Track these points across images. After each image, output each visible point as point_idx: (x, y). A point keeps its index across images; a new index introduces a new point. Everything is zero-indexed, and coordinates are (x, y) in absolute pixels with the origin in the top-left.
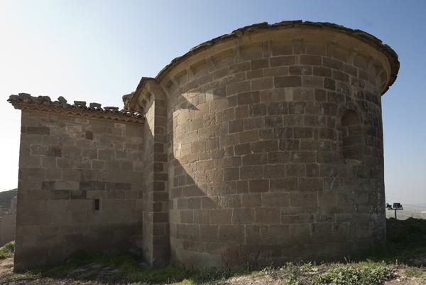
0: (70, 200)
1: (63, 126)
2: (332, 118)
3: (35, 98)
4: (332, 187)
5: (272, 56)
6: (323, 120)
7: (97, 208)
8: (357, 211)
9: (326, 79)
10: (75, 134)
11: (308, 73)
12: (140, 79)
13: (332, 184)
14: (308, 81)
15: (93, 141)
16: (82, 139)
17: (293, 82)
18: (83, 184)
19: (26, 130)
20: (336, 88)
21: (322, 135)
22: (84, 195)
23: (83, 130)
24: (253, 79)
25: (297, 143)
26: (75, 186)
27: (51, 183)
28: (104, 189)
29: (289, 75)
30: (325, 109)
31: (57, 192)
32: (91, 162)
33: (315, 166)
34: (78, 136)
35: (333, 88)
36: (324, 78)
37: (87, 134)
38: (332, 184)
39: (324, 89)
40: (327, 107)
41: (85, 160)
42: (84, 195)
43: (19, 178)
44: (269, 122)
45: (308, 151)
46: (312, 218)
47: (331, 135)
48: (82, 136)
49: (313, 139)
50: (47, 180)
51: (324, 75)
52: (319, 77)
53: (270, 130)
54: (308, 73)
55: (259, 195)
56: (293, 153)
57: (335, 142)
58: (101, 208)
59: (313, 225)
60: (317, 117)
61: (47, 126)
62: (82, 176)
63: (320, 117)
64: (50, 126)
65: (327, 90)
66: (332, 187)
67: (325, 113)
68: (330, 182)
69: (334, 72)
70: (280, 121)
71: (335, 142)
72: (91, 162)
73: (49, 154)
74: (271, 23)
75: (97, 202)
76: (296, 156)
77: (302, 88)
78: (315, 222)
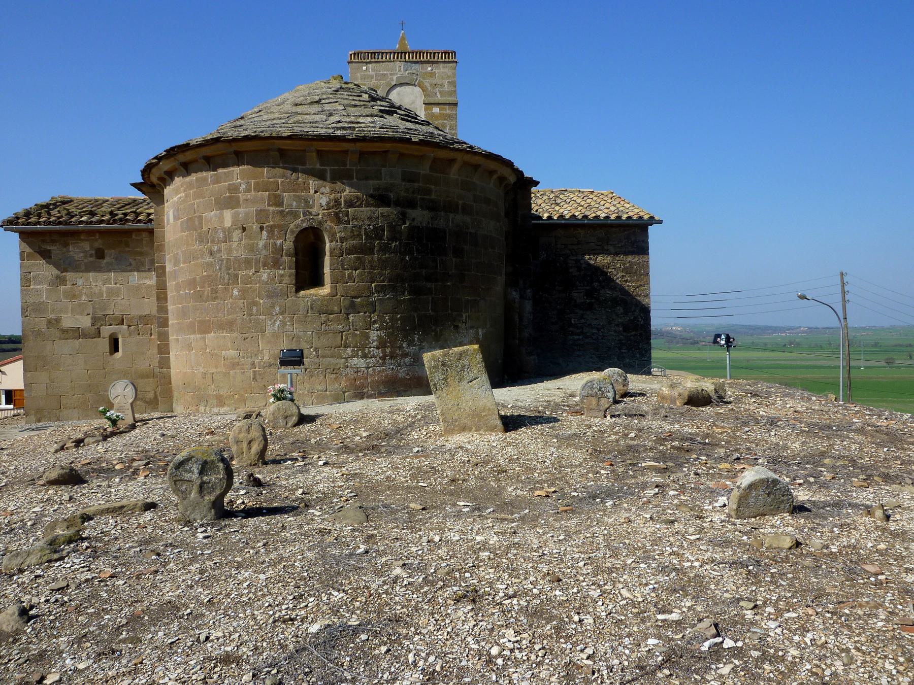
6: (265, 246)
9: (269, 194)
10: (82, 255)
11: (248, 190)
12: (140, 173)
13: (278, 323)
14: (247, 200)
15: (105, 261)
16: (91, 259)
18: (95, 320)
21: (264, 265)
22: (98, 334)
23: (91, 247)
25: (237, 276)
26: (85, 322)
27: (58, 320)
28: (123, 324)
29: (228, 194)
30: (268, 233)
31: (65, 331)
32: (104, 289)
33: (255, 303)
34: (85, 257)
35: (281, 204)
37: (96, 253)
38: (278, 323)
39: (267, 208)
44: (211, 253)
46: (253, 364)
47: (276, 264)
48: (91, 256)
53: (212, 262)
54: (248, 190)
55: (204, 338)
56: (233, 289)
59: (254, 372)
60: (257, 244)
61: (48, 248)
62: (94, 308)
67: (269, 238)
68: (275, 321)
69: (282, 182)
70: (219, 251)
72: (104, 289)
73: (52, 283)
74: (194, 143)
76: (235, 292)
77: (240, 210)
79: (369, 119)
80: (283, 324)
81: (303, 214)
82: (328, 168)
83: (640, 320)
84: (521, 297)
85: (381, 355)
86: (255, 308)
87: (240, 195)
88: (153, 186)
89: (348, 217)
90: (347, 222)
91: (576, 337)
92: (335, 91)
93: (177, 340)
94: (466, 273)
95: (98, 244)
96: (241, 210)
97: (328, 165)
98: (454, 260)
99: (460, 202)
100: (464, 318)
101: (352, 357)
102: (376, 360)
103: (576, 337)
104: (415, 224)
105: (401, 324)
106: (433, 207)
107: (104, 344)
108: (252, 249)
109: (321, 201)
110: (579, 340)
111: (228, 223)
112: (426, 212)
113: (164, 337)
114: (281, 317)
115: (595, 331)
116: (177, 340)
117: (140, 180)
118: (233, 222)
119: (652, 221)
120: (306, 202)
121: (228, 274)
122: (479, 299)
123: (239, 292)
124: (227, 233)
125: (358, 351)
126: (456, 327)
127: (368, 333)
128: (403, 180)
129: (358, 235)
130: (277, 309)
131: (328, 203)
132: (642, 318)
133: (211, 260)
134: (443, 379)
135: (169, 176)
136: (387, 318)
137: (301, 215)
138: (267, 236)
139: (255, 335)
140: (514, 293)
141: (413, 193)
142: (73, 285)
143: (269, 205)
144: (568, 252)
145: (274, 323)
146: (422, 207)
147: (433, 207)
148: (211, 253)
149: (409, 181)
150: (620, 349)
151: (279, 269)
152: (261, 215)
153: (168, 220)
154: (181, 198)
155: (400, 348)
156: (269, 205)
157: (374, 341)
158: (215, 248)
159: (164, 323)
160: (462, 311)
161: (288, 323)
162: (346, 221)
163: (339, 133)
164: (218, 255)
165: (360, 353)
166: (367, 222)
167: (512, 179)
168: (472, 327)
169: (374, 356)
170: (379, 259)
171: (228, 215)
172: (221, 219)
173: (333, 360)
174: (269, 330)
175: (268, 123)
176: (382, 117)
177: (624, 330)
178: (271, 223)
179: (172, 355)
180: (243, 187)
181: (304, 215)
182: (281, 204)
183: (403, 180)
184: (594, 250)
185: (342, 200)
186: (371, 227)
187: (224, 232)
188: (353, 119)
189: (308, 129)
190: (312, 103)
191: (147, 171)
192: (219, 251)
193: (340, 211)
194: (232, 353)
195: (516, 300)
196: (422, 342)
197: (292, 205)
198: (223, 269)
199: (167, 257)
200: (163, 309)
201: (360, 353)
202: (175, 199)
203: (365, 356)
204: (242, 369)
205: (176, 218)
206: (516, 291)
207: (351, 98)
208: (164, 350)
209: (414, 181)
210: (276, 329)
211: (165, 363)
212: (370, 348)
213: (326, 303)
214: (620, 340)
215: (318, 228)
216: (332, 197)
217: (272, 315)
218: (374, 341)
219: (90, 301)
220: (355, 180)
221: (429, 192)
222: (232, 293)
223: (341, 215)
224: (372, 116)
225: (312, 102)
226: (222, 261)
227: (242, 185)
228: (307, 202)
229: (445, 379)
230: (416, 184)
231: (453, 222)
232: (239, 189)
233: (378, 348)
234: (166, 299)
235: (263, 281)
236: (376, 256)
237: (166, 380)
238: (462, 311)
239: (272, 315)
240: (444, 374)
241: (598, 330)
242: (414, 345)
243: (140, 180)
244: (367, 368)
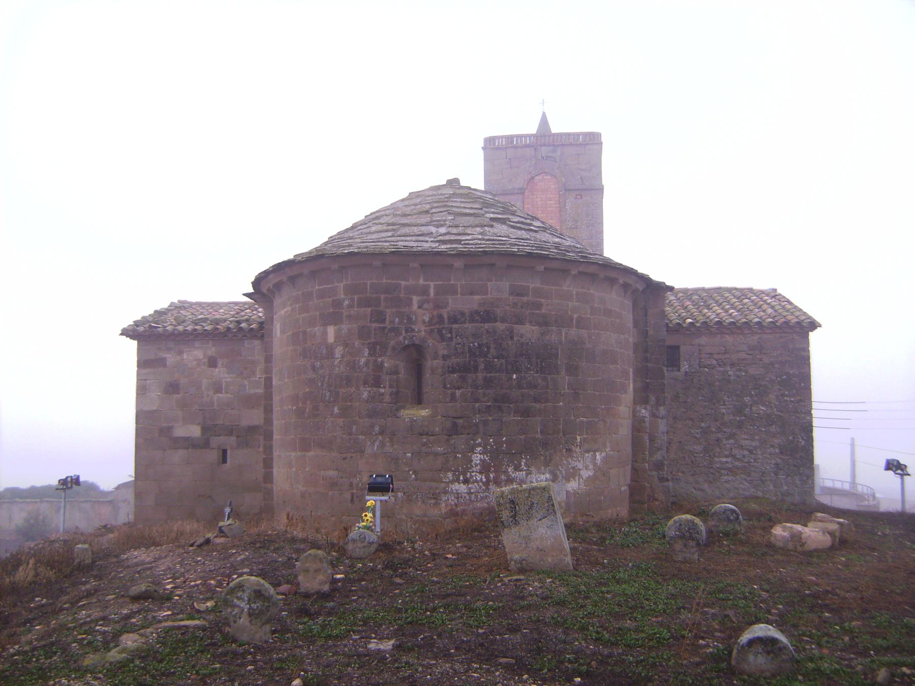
0: (190, 450)
1: (180, 353)
2: (380, 360)
3: (49, 487)
4: (376, 447)
5: (317, 287)
6: (367, 363)
7: (224, 460)
8: (416, 479)
11: (351, 306)
12: (251, 285)
13: (377, 443)
17: (334, 318)
18: (205, 429)
19: (143, 364)
20: (387, 320)
21: (365, 383)
23: (205, 355)
24: (303, 315)
26: (195, 431)
27: (170, 429)
29: (331, 310)
30: (370, 350)
31: (176, 440)
36: (369, 309)
38: (377, 443)
40: (372, 348)
41: (208, 396)
42: (205, 444)
43: (137, 423)
45: (349, 404)
48: (204, 365)
49: (353, 389)
50: (165, 425)
51: (369, 307)
52: (363, 309)
57: (382, 390)
58: (228, 461)
59: (352, 494)
63: (363, 360)
64: (168, 356)
65: (374, 325)
66: (376, 447)
68: (374, 441)
71: (382, 390)
75: (225, 452)
76: (336, 410)
77: (343, 326)
78: (355, 491)
79: (478, 229)
80: (383, 445)
81: (405, 330)
82: (432, 284)
83: (801, 440)
84: (654, 415)
85: (484, 480)
86: (354, 427)
87: (343, 311)
88: (264, 295)
89: (452, 335)
90: (451, 339)
91: (724, 460)
92: (447, 198)
93: (280, 456)
94: (581, 392)
95: (212, 351)
96: (345, 327)
97: (432, 282)
98: (567, 377)
99: (575, 316)
100: (579, 440)
101: (452, 482)
102: (478, 485)
103: (724, 460)
104: (523, 340)
105: (506, 448)
106: (544, 323)
107: (213, 456)
108: (353, 366)
109: (424, 318)
110: (727, 462)
111: (331, 339)
112: (535, 328)
113: (269, 450)
114: (380, 437)
115: (746, 453)
116: (280, 456)
117: (251, 290)
118: (335, 338)
119: (820, 326)
120: (409, 318)
121: (330, 391)
122: (596, 420)
123: (339, 410)
124: (329, 349)
125: (459, 475)
126: (569, 450)
127: (471, 456)
128: (511, 294)
129: (462, 353)
130: (377, 429)
131: (431, 319)
132: (803, 439)
133: (314, 376)
134: (511, 517)
135: (278, 286)
136: (491, 440)
137: (404, 332)
138: (369, 354)
139: (354, 455)
140: (643, 411)
141: (522, 307)
142: (186, 393)
143: (371, 321)
144: (714, 362)
145: (373, 444)
146: (531, 322)
147: (544, 323)
148: (314, 368)
149: (517, 295)
150: (776, 474)
151: (380, 387)
152: (363, 333)
153: (276, 333)
154: (287, 311)
155: (506, 472)
156: (371, 321)
157: (476, 465)
158: (318, 364)
159: (269, 436)
160: (576, 434)
161: (388, 444)
162: (449, 338)
163: (443, 247)
164: (321, 372)
165: (461, 478)
166: (471, 340)
167: (640, 287)
168: (588, 451)
169: (476, 481)
170: (485, 378)
171: (331, 330)
172: (325, 333)
173: (433, 484)
174: (368, 451)
175: (374, 236)
176: (492, 226)
177: (782, 453)
178: (374, 340)
179: (275, 470)
180: (347, 302)
181: (407, 331)
182: (383, 321)
183: (511, 294)
184: (743, 360)
185: (445, 316)
186: (476, 344)
187: (327, 348)
188: (460, 230)
189: (412, 244)
190: (421, 213)
191: (257, 283)
192: (322, 367)
193: (443, 328)
194: (332, 473)
195: (646, 419)
196: (529, 467)
197: (394, 322)
198: (325, 385)
199: (274, 370)
200: (269, 421)
201: (461, 478)
202: (283, 312)
203: (466, 481)
204: (340, 490)
205: (282, 332)
206: (645, 409)
207: (462, 205)
208: (268, 463)
209: (522, 295)
210: (375, 449)
211: (268, 477)
212: (473, 472)
213: (426, 423)
214: (776, 464)
215: (420, 346)
216: (435, 313)
217: (371, 434)
218: (476, 465)
219: (201, 410)
220: (459, 296)
221: (539, 306)
222: (333, 411)
223: (444, 332)
224: (482, 226)
225: (421, 212)
226: (324, 377)
227: (345, 301)
228: (409, 319)
229: (514, 517)
230: (525, 299)
231: (566, 337)
232: (342, 305)
233: (480, 473)
234: (272, 411)
235: (363, 399)
236: (480, 376)
237: (269, 494)
238: (576, 434)
239: (371, 434)
240: (512, 511)
241: (751, 452)
242: (521, 470)
243: (251, 290)
244: (470, 493)
